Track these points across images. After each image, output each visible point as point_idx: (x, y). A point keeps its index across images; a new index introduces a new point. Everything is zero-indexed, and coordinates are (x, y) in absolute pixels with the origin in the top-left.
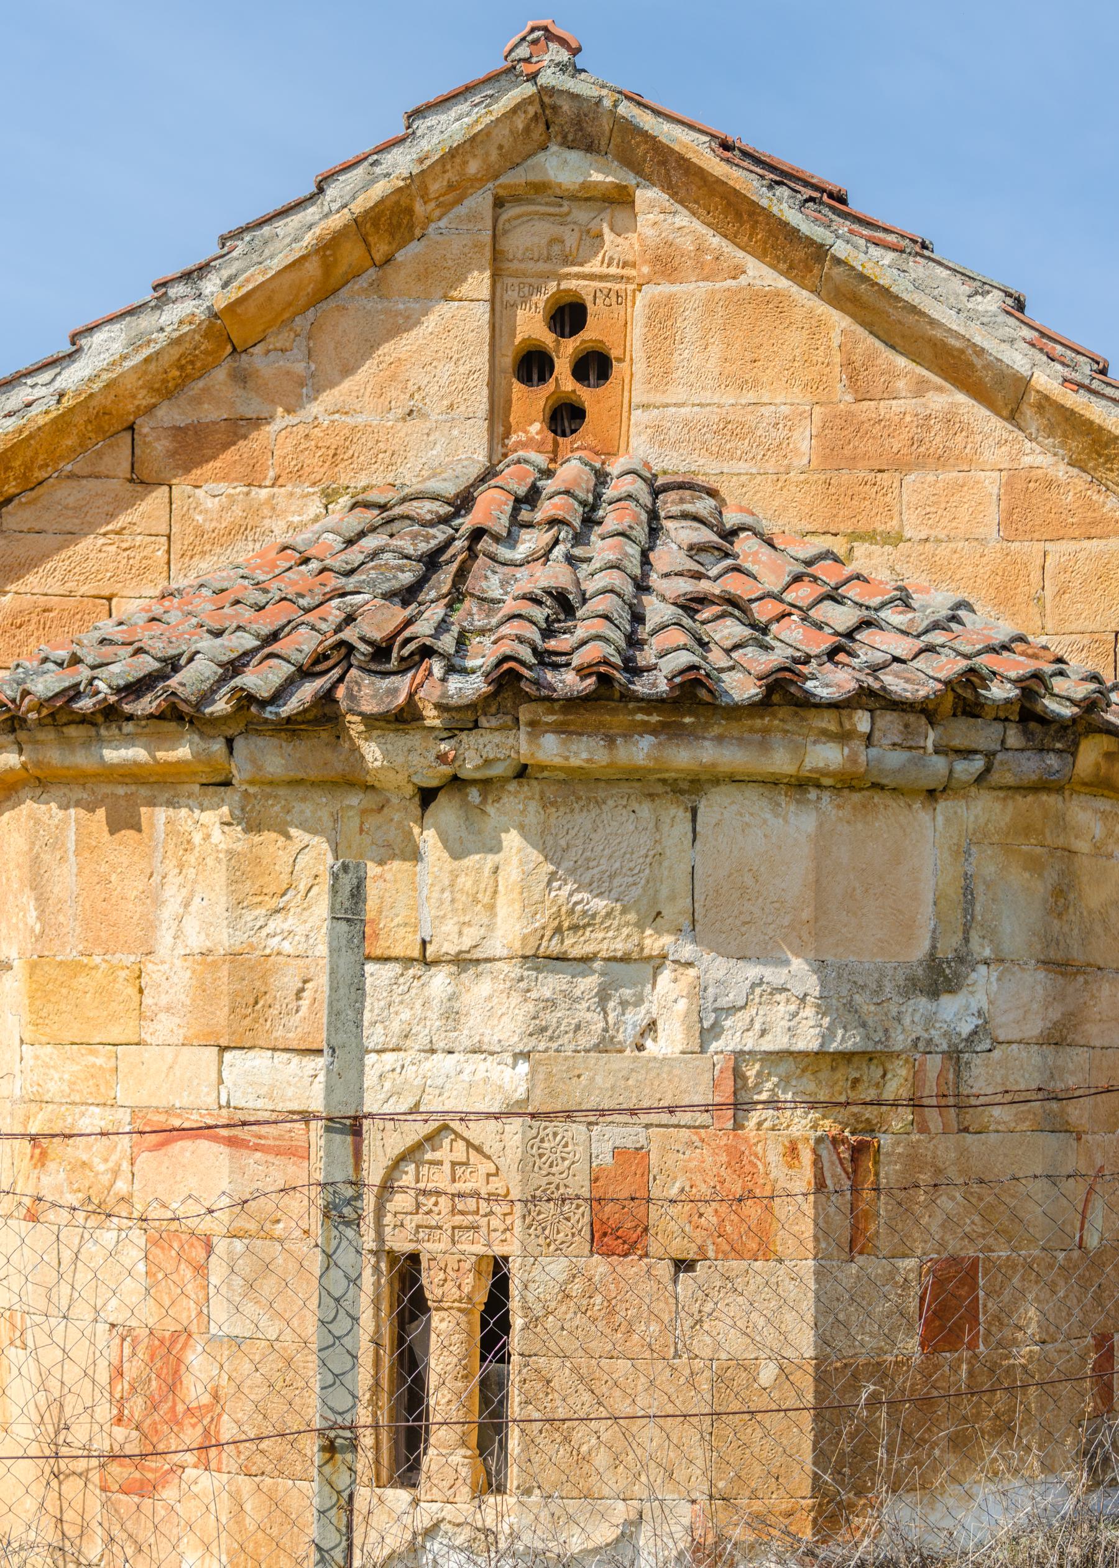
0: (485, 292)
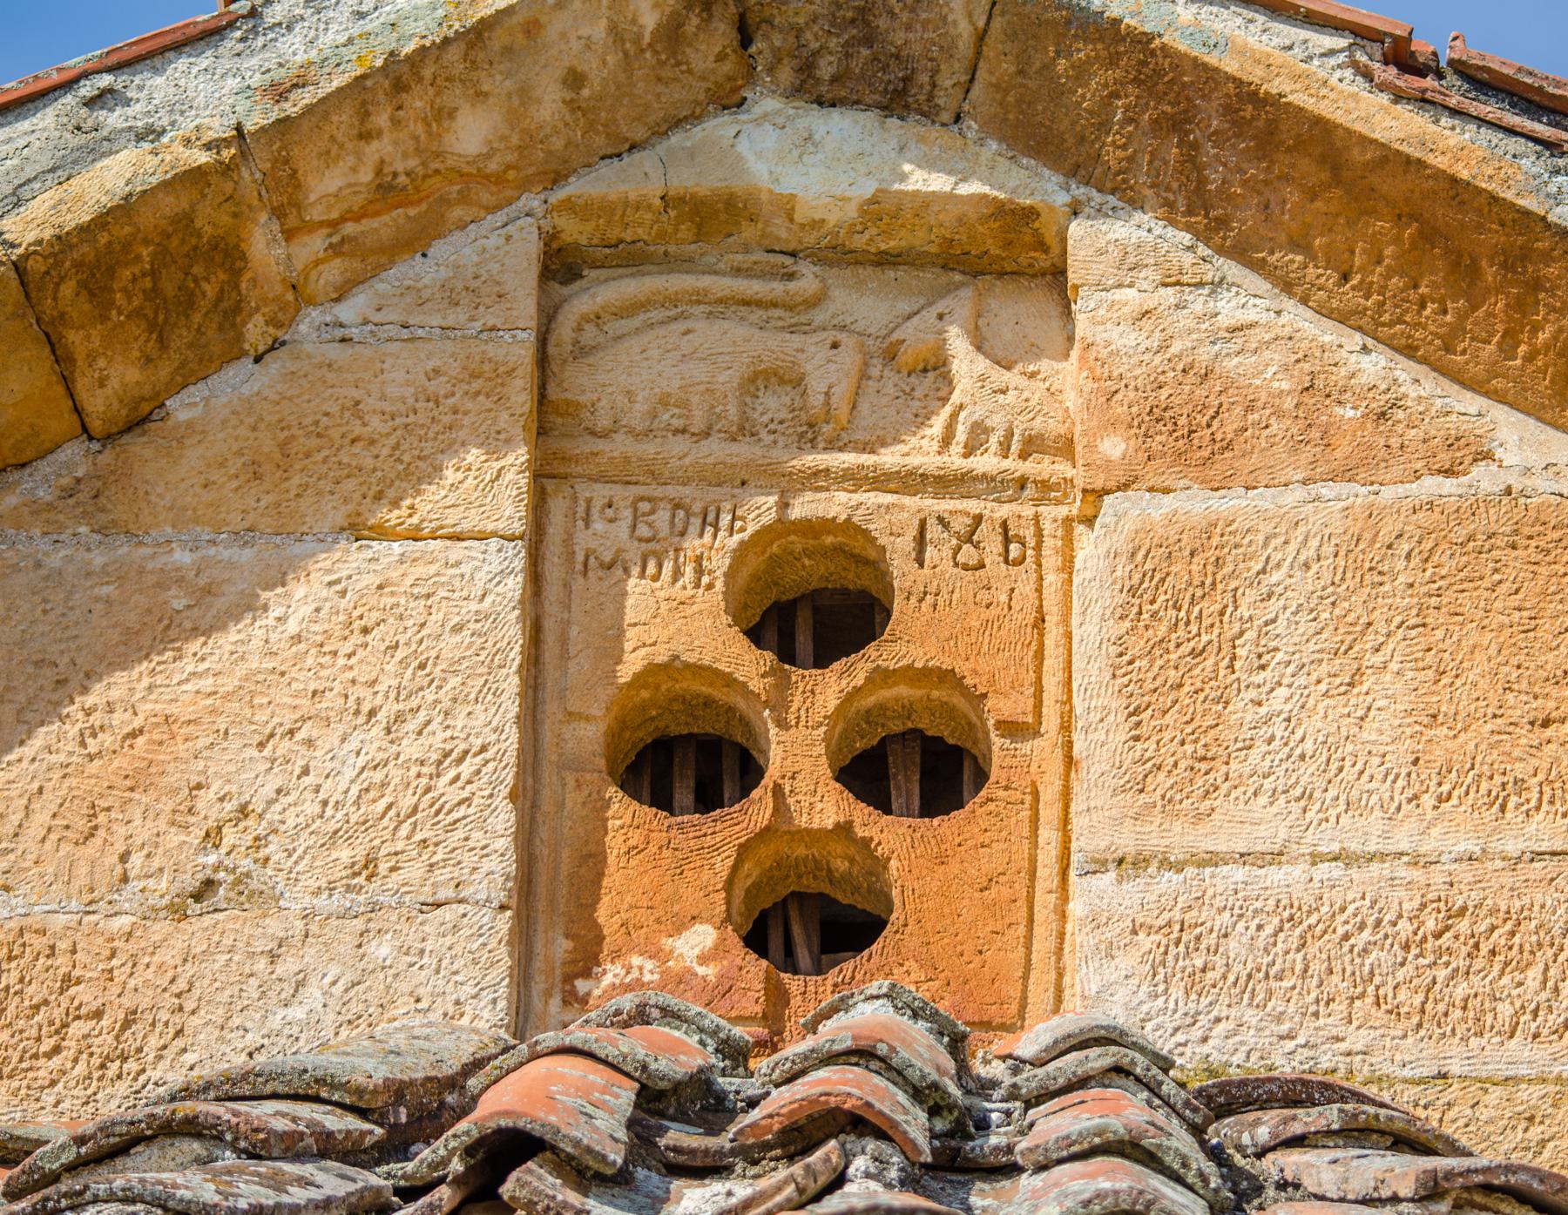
0: (508, 507)
